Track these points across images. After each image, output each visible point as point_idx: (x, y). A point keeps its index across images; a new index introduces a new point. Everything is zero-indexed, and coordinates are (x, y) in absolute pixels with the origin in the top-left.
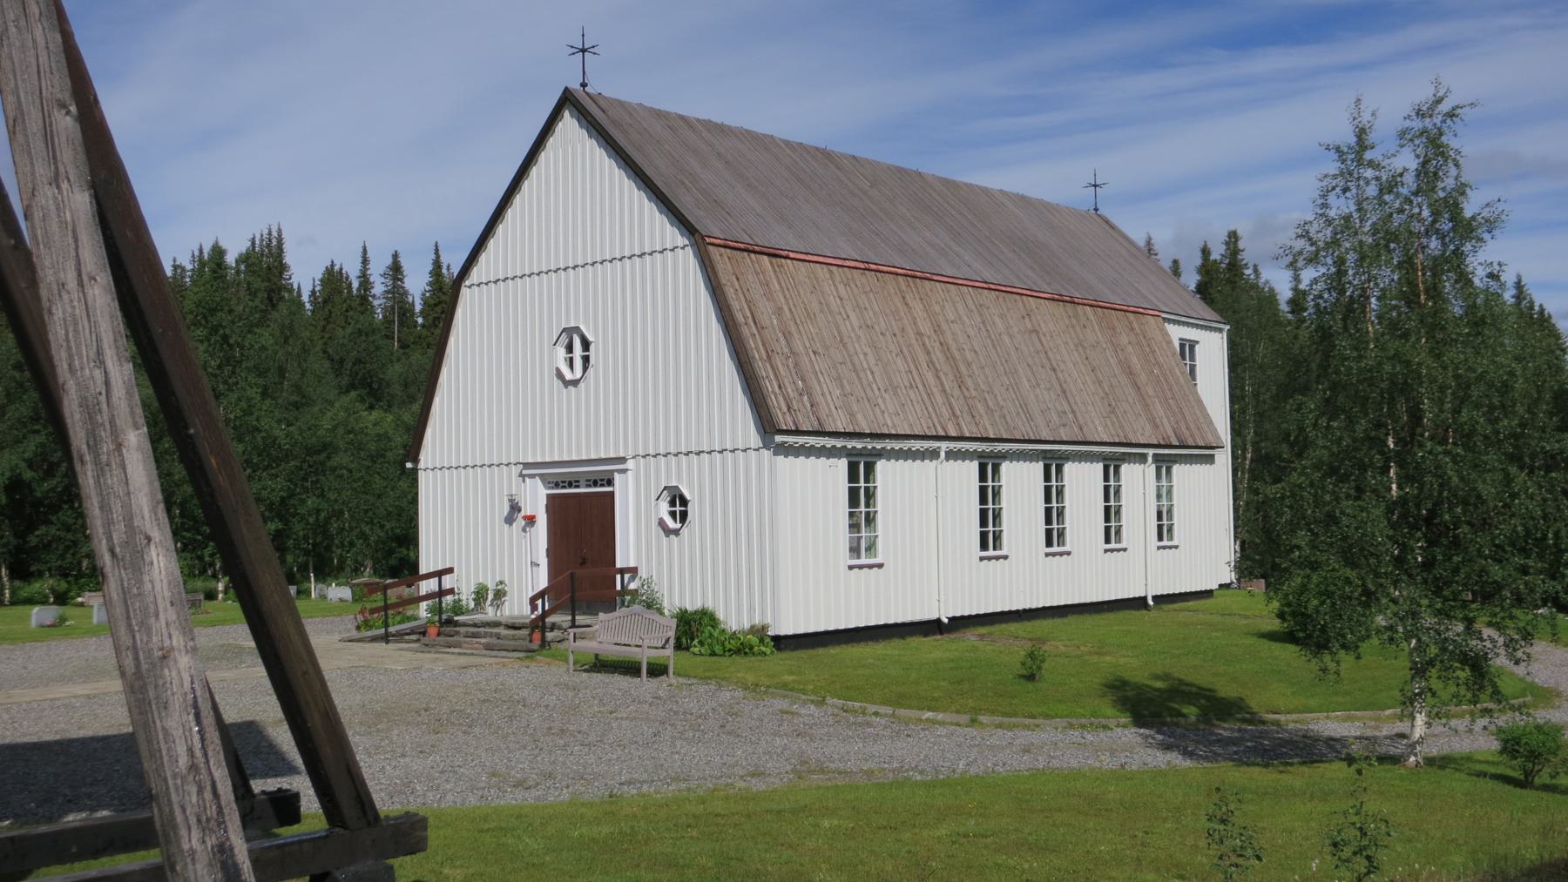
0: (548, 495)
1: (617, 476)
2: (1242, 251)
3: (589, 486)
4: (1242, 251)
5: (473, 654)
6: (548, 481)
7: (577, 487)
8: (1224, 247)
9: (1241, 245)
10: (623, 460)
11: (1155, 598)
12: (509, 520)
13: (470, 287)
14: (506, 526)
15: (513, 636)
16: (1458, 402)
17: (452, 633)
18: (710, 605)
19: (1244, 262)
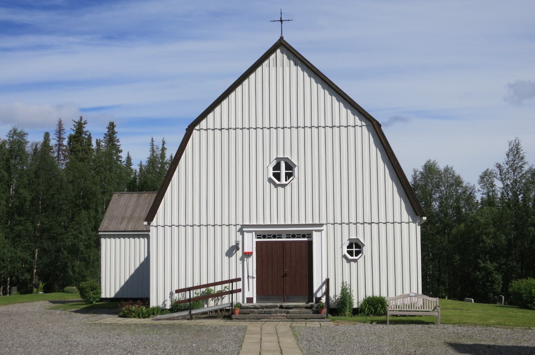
0: (257, 242)
1: (314, 233)
2: (116, 133)
3: (287, 238)
4: (116, 133)
5: (273, 321)
6: (258, 236)
7: (281, 238)
8: (107, 130)
9: (116, 129)
10: (321, 225)
11: (445, 298)
12: (230, 254)
13: (199, 130)
14: (226, 258)
15: (299, 312)
16: (76, 218)
17: (248, 312)
18: (384, 295)
19: (117, 138)
